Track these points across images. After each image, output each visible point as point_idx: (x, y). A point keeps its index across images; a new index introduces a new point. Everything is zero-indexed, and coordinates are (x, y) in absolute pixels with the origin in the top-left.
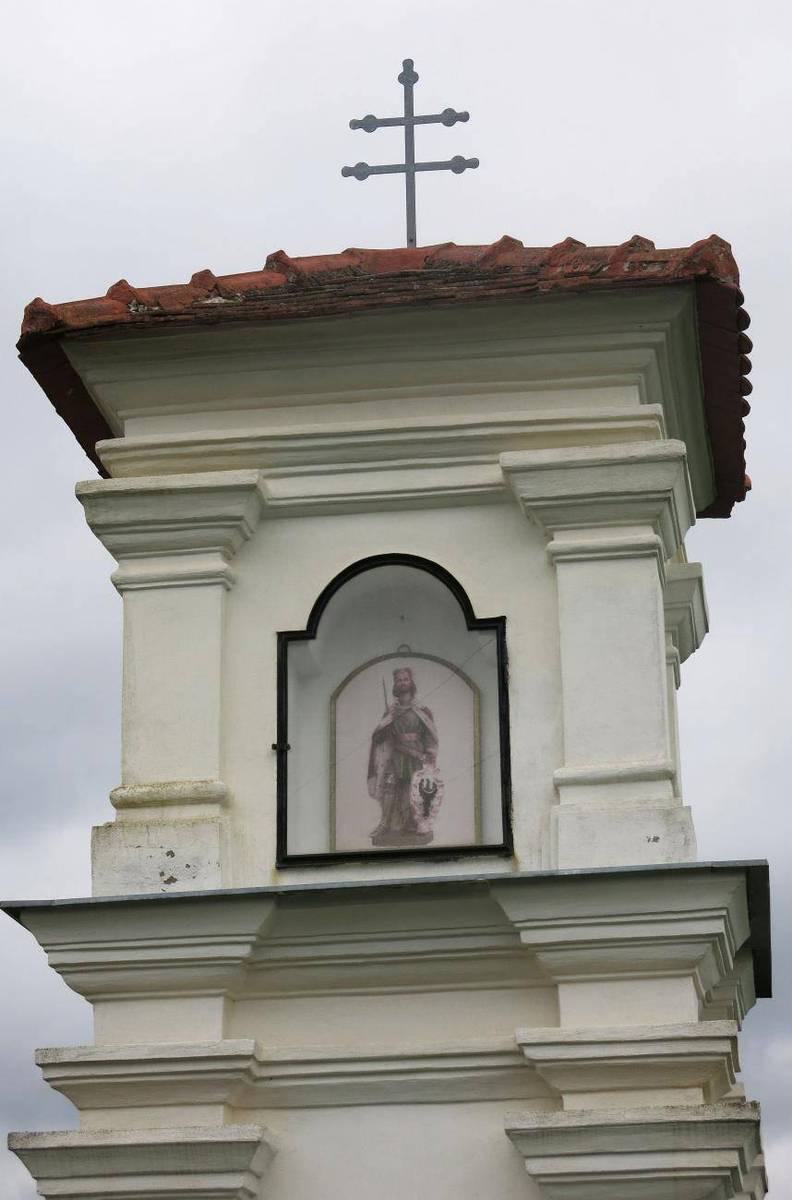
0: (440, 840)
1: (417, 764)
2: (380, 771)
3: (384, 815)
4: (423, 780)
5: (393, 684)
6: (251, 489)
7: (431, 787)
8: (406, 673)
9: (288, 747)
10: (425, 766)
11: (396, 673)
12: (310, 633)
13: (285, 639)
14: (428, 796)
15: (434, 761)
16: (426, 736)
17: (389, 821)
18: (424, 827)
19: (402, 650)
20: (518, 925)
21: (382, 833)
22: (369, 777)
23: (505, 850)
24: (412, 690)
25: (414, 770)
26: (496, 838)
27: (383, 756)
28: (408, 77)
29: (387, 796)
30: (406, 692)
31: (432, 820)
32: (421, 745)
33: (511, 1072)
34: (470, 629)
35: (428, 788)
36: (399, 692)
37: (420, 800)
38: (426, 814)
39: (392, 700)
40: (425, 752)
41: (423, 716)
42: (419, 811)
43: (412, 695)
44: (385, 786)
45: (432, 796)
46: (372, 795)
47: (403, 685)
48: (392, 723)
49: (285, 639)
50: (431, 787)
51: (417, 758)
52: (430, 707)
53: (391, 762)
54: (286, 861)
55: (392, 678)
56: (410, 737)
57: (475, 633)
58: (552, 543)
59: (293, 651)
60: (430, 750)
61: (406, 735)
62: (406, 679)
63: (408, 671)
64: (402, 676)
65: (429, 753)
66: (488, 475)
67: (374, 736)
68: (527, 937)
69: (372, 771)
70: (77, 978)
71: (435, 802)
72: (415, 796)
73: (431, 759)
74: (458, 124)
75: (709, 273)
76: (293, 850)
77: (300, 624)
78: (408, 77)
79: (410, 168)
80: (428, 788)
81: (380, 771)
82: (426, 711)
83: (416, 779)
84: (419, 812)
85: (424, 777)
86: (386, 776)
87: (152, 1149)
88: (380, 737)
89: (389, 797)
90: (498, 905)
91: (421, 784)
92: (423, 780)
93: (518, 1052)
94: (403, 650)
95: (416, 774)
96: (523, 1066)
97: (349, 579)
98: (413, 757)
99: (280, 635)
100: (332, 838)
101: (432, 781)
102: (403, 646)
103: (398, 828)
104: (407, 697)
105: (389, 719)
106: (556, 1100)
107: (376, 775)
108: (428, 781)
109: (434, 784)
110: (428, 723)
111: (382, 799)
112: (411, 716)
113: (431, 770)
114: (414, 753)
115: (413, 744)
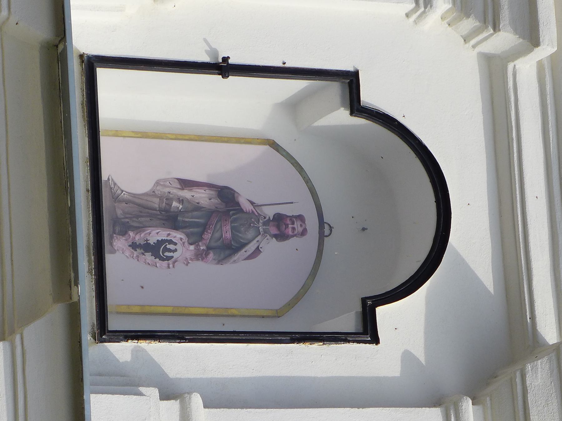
0: (109, 259)
2: (186, 194)
3: (134, 195)
4: (175, 244)
5: (290, 214)
6: (268, 228)
7: (167, 254)
8: (300, 229)
9: (225, 76)
10: (192, 247)
11: (300, 218)
15: (198, 260)
17: (127, 202)
19: (326, 226)
20: (18, 338)
22: (178, 179)
24: (281, 237)
25: (188, 235)
26: (114, 324)
29: (157, 200)
30: (278, 227)
31: (127, 253)
32: (219, 243)
34: (364, 301)
35: (166, 250)
36: (279, 219)
37: (153, 240)
38: (134, 246)
39: (270, 212)
40: (209, 248)
41: (251, 248)
42: (139, 238)
43: (276, 236)
44: (169, 200)
45: (156, 255)
46: (158, 183)
47: (287, 226)
48: (241, 211)
50: (167, 254)
51: (201, 239)
52: (260, 257)
53: (198, 208)
55: (296, 213)
57: (359, 308)
58: (470, 402)
60: (211, 255)
61: (228, 227)
62: (294, 229)
63: (304, 233)
64: (297, 225)
65: (207, 254)
69: (185, 184)
71: (149, 257)
73: (200, 256)
80: (166, 250)
81: (186, 194)
82: (257, 251)
83: (177, 236)
84: (137, 238)
85: (179, 247)
86: (181, 201)
89: (156, 203)
91: (171, 242)
92: (175, 244)
94: (327, 231)
95: (183, 236)
98: (202, 233)
99: (356, 74)
100: (117, 134)
101: (175, 255)
102: (331, 228)
103: (119, 212)
104: (274, 230)
105: (247, 207)
107: (183, 189)
108: (176, 250)
109: (172, 257)
110: (242, 254)
111: (152, 193)
112: (250, 234)
113: (188, 255)
114: (207, 236)
115: (217, 235)
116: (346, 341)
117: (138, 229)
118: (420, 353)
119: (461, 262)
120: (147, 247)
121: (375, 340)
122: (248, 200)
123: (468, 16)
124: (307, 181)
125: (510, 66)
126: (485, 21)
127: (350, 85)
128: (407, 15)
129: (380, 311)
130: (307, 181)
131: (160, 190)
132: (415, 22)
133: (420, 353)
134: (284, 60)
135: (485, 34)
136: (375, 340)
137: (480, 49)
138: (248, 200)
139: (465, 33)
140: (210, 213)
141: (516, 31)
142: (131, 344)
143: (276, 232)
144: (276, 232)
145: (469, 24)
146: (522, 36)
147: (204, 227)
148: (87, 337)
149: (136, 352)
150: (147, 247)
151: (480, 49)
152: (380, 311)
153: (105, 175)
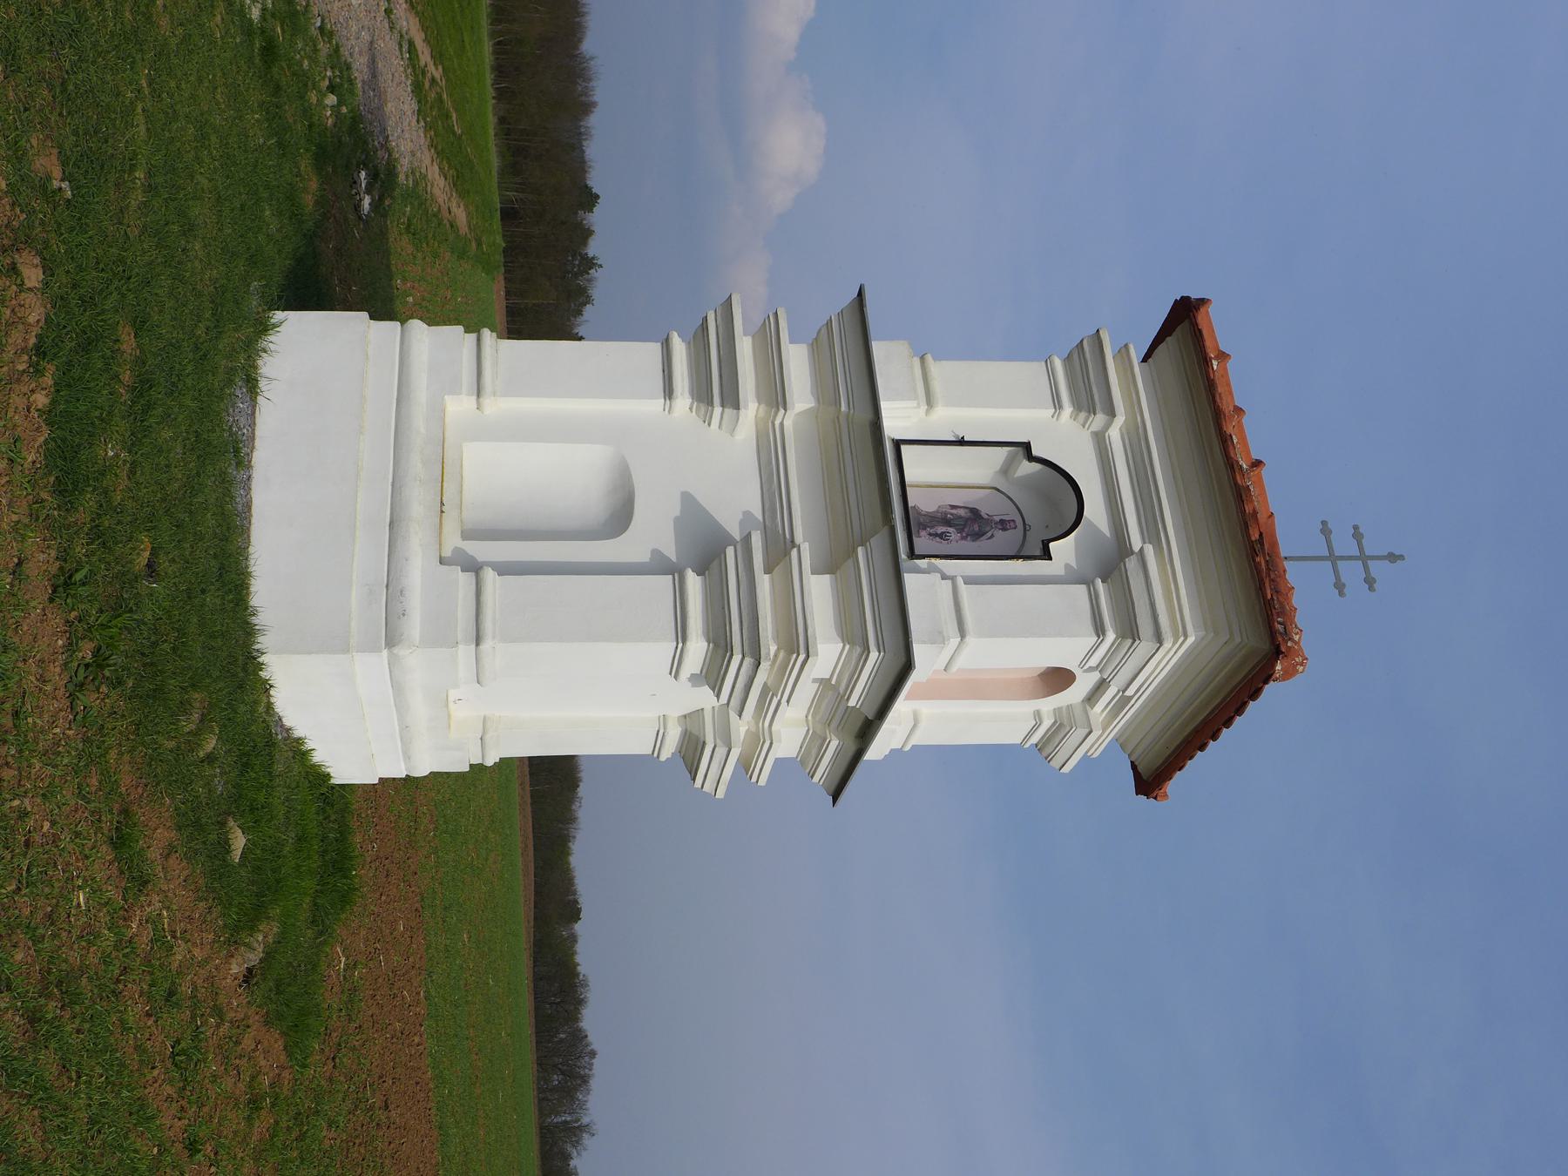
0: (915, 539)
1: (960, 531)
2: (954, 511)
12: (1031, 457)
13: (1026, 447)
14: (942, 536)
16: (977, 536)
18: (923, 533)
21: (919, 513)
23: (912, 555)
24: (1004, 529)
26: (917, 552)
27: (962, 512)
28: (1393, 557)
33: (782, 537)
35: (946, 536)
37: (939, 532)
38: (930, 534)
39: (997, 519)
41: (989, 534)
43: (1002, 529)
44: (946, 514)
46: (939, 507)
49: (1026, 447)
52: (994, 539)
53: (960, 517)
54: (898, 444)
56: (976, 528)
58: (1100, 580)
59: (1020, 450)
64: (1012, 524)
66: (1136, 542)
67: (977, 510)
68: (860, 550)
70: (824, 331)
72: (940, 529)
73: (963, 538)
74: (1367, 586)
75: (1283, 653)
76: (904, 448)
77: (1035, 452)
78: (1393, 557)
79: (1333, 558)
80: (946, 536)
81: (954, 511)
82: (992, 536)
83: (950, 530)
86: (952, 514)
87: (756, 628)
88: (975, 513)
90: (876, 533)
93: (793, 544)
94: (1028, 528)
96: (785, 549)
97: (1061, 475)
100: (912, 486)
105: (986, 517)
106: (768, 570)
110: (985, 537)
111: (937, 512)
116: (1035, 559)
117: (932, 527)
118: (1074, 564)
119: (1091, 524)
120: (936, 535)
121: (1050, 559)
122: (860, 294)
123: (1081, 411)
124: (1015, 504)
125: (1107, 435)
126: (1089, 412)
127: (1027, 448)
128: (1053, 417)
129: (1052, 545)
130: (1015, 504)
131: (941, 510)
132: (1057, 419)
133: (1074, 564)
134: (1164, 803)
135: (1091, 419)
136: (1050, 559)
137: (1092, 429)
138: (860, 294)
139: (1082, 422)
140: (967, 520)
141: (1104, 413)
142: (926, 561)
143: (1000, 527)
144: (1000, 527)
145: (1083, 415)
146: (1108, 415)
147: (965, 526)
148: (903, 556)
149: (928, 563)
150: (936, 535)
151: (1090, 431)
152: (1052, 545)
153: (911, 504)
